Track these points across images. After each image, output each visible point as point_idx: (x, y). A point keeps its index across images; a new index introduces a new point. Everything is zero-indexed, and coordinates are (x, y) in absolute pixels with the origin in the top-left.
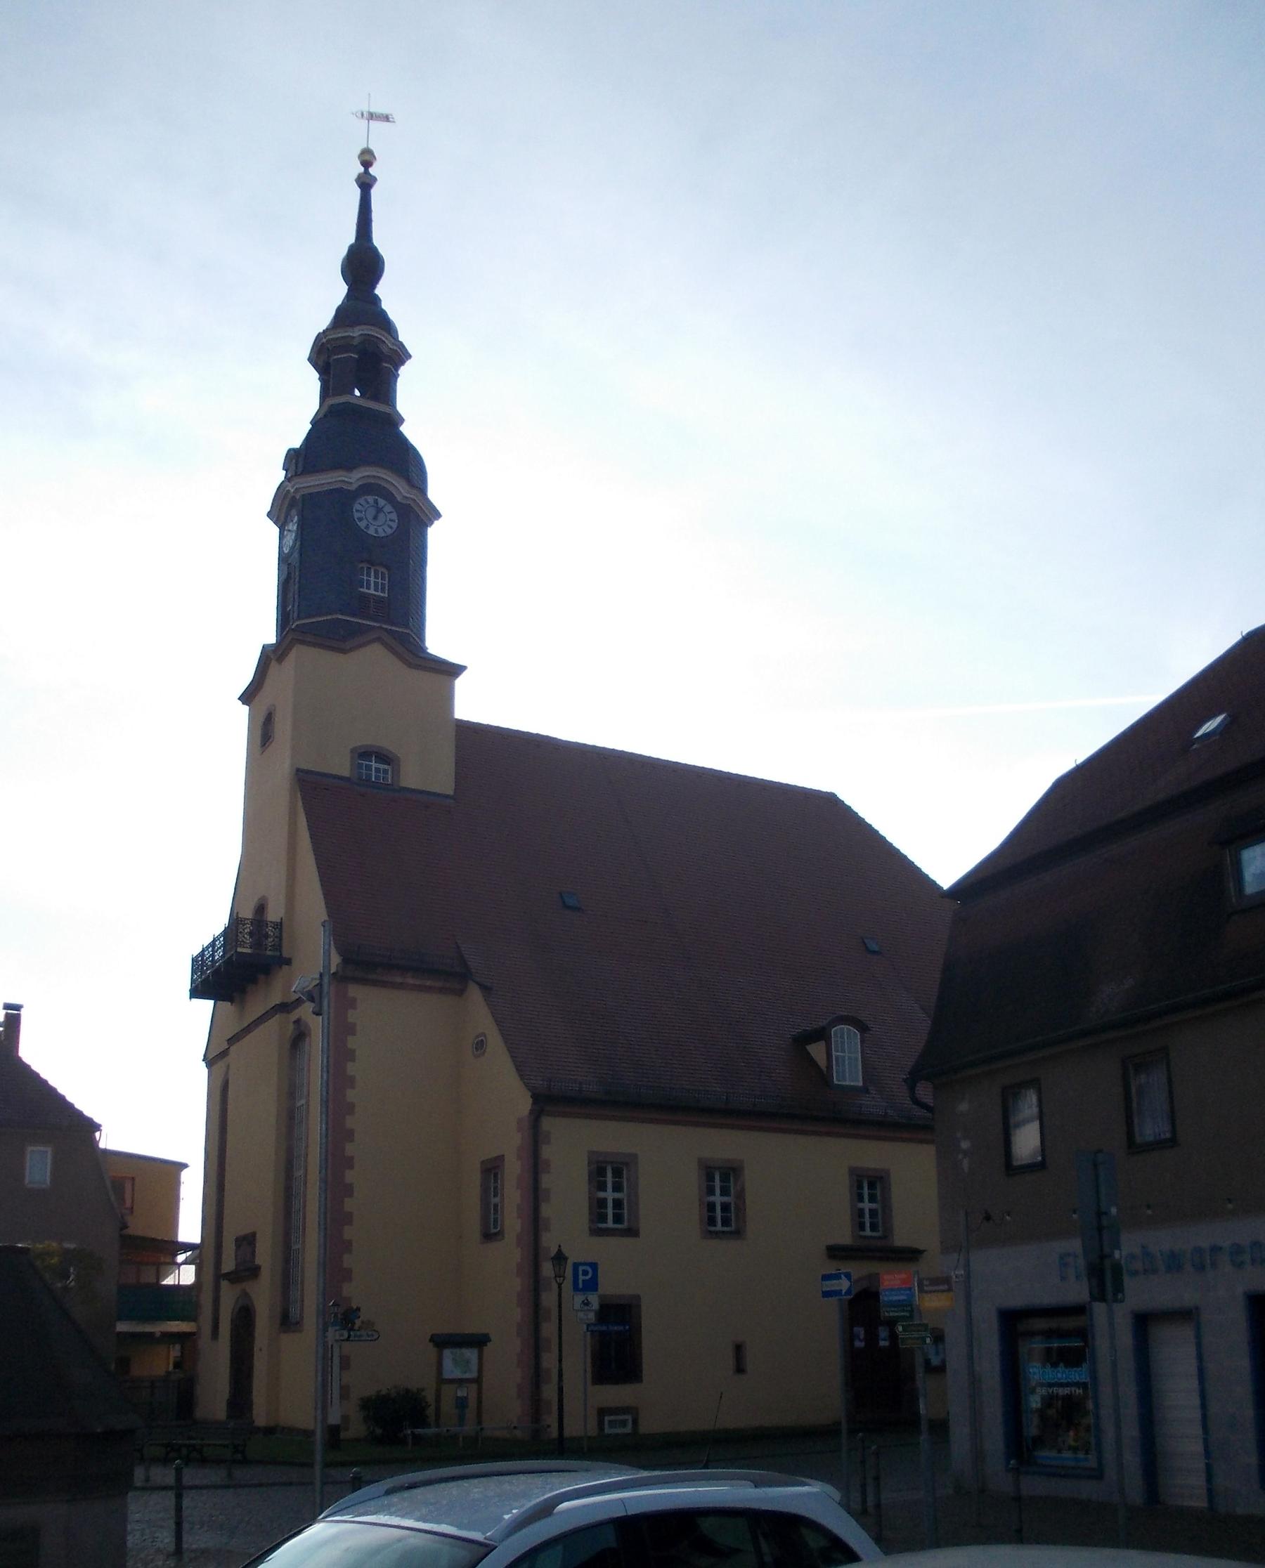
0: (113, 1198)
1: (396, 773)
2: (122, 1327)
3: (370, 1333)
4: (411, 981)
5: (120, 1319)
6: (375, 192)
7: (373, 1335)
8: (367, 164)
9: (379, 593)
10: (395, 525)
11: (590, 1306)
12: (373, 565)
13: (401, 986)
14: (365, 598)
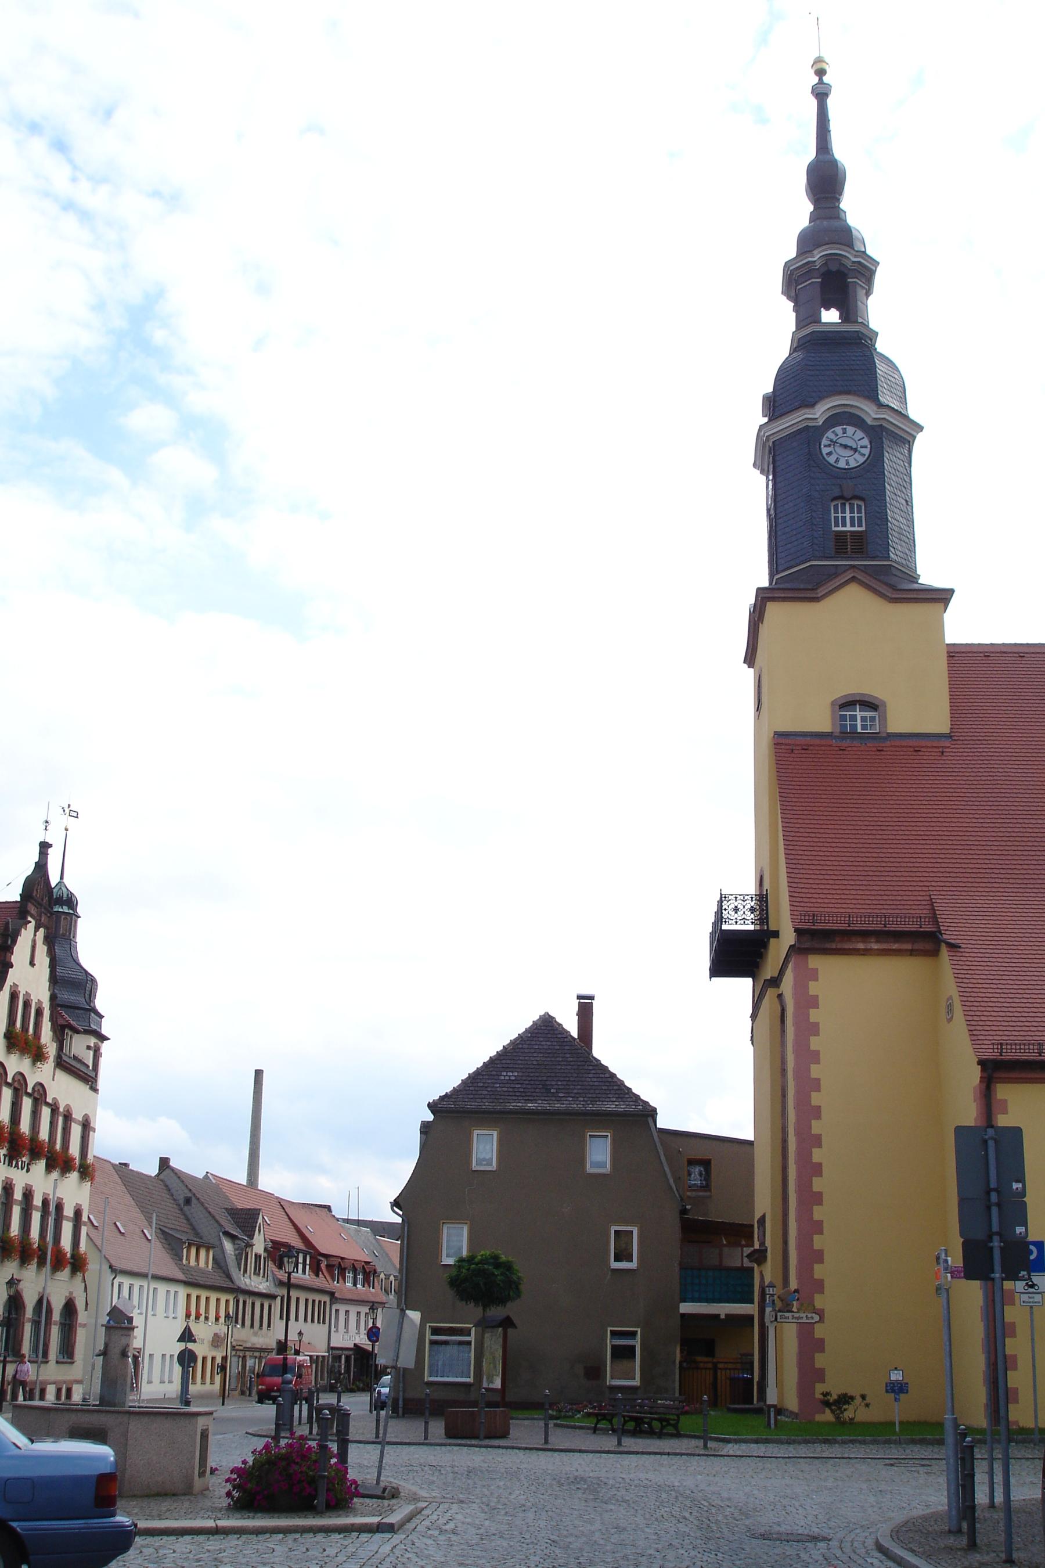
0: (671, 1181)
1: (883, 719)
2: (686, 1308)
3: (809, 1315)
4: (875, 946)
5: (684, 1300)
6: (830, 102)
7: (812, 1318)
8: (821, 73)
9: (856, 529)
10: (866, 451)
11: (1036, 1288)
12: (848, 500)
13: (866, 952)
14: (840, 537)
